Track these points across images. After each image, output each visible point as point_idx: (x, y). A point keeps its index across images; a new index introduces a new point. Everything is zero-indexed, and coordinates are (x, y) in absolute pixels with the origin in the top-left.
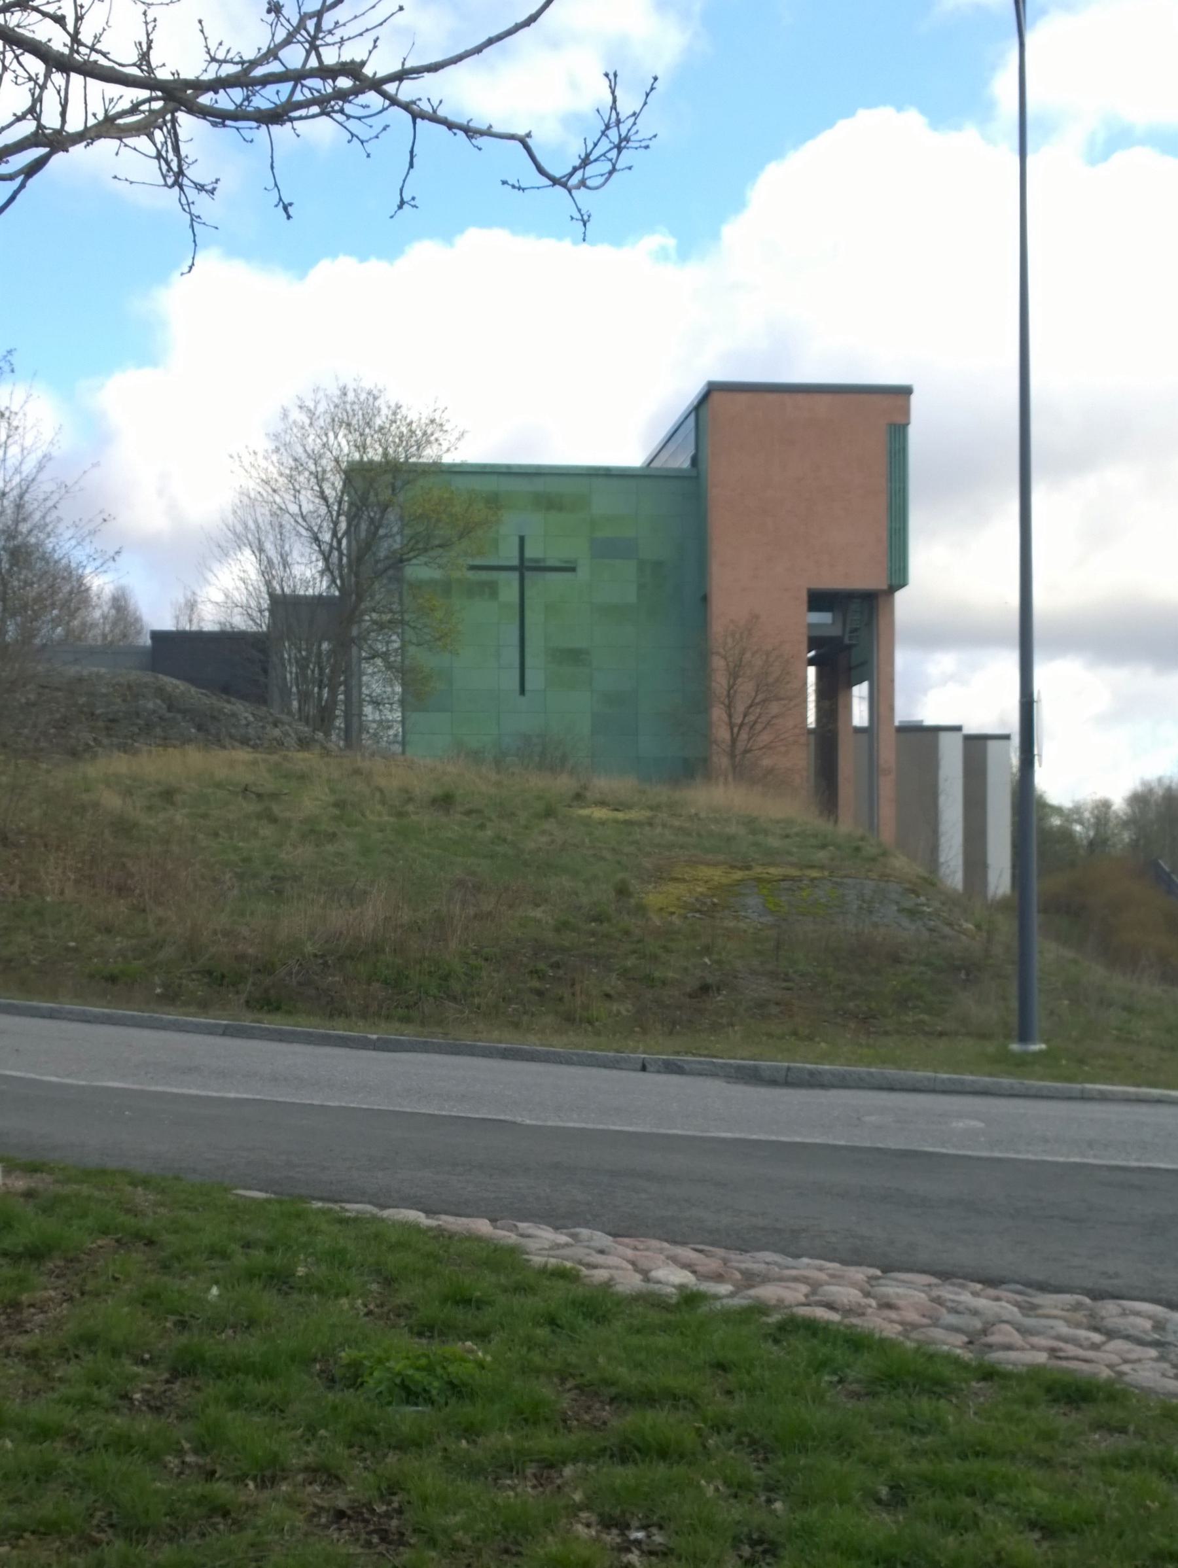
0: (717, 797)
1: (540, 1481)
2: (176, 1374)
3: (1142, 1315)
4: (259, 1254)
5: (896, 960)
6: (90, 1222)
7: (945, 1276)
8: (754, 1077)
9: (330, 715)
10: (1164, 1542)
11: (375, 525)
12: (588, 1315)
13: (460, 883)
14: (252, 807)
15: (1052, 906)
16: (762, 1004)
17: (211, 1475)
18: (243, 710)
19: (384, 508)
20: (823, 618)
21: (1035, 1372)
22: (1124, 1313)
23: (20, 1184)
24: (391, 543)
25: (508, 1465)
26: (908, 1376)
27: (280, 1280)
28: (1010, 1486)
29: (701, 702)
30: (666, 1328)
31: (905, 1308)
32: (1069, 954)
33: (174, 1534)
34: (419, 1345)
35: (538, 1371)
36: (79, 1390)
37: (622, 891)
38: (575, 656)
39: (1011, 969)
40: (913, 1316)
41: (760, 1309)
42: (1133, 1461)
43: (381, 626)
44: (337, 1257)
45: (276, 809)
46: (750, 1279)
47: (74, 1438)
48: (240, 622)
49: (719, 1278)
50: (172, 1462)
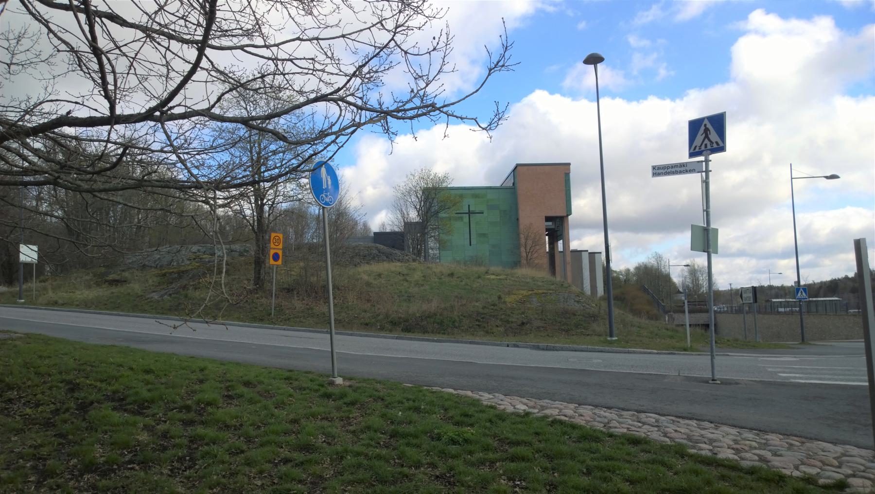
0: (523, 272)
1: (491, 467)
2: (392, 437)
3: (652, 418)
4: (411, 403)
5: (575, 315)
6: (366, 394)
7: (596, 406)
8: (538, 348)
9: (420, 252)
10: (664, 486)
11: (431, 204)
12: (500, 419)
13: (457, 297)
14: (401, 278)
15: (616, 298)
16: (538, 327)
17: (402, 466)
18: (397, 252)
19: (433, 199)
20: (550, 223)
21: (623, 435)
22: (647, 417)
23: (348, 383)
24: (435, 208)
25: (482, 462)
26: (588, 436)
27: (417, 410)
28: (620, 469)
29: (518, 246)
30: (521, 423)
31: (586, 416)
32: (622, 312)
33: (394, 483)
34: (455, 428)
35: (488, 435)
36: (367, 442)
37: (500, 298)
38: (484, 235)
39: (606, 317)
40: (588, 419)
41: (546, 417)
42: (654, 462)
43: (433, 229)
44: (432, 403)
45: (408, 278)
46: (543, 408)
47: (366, 455)
48: (397, 230)
49: (534, 408)
50: (392, 462)
